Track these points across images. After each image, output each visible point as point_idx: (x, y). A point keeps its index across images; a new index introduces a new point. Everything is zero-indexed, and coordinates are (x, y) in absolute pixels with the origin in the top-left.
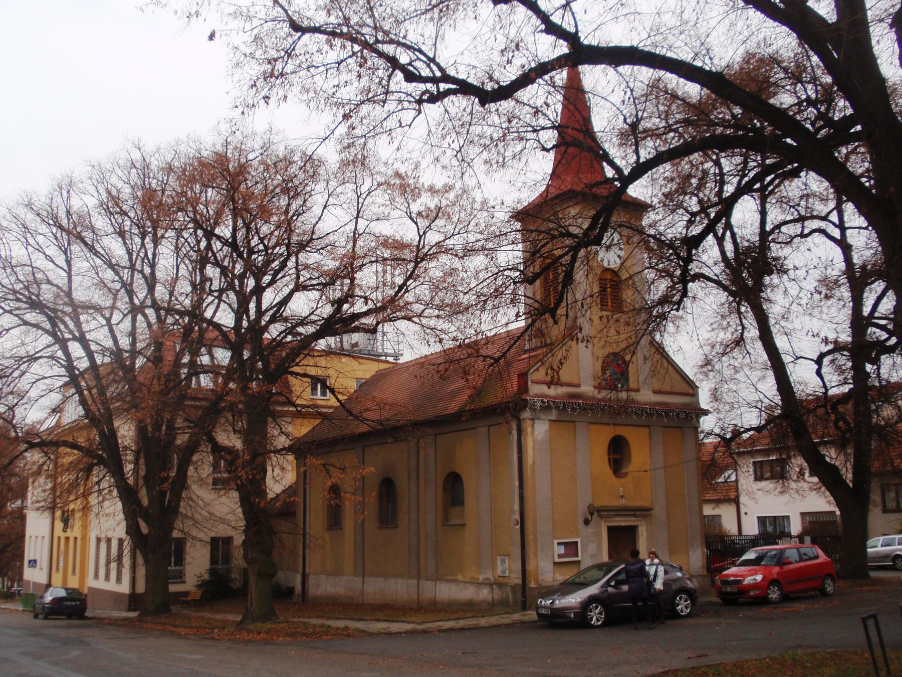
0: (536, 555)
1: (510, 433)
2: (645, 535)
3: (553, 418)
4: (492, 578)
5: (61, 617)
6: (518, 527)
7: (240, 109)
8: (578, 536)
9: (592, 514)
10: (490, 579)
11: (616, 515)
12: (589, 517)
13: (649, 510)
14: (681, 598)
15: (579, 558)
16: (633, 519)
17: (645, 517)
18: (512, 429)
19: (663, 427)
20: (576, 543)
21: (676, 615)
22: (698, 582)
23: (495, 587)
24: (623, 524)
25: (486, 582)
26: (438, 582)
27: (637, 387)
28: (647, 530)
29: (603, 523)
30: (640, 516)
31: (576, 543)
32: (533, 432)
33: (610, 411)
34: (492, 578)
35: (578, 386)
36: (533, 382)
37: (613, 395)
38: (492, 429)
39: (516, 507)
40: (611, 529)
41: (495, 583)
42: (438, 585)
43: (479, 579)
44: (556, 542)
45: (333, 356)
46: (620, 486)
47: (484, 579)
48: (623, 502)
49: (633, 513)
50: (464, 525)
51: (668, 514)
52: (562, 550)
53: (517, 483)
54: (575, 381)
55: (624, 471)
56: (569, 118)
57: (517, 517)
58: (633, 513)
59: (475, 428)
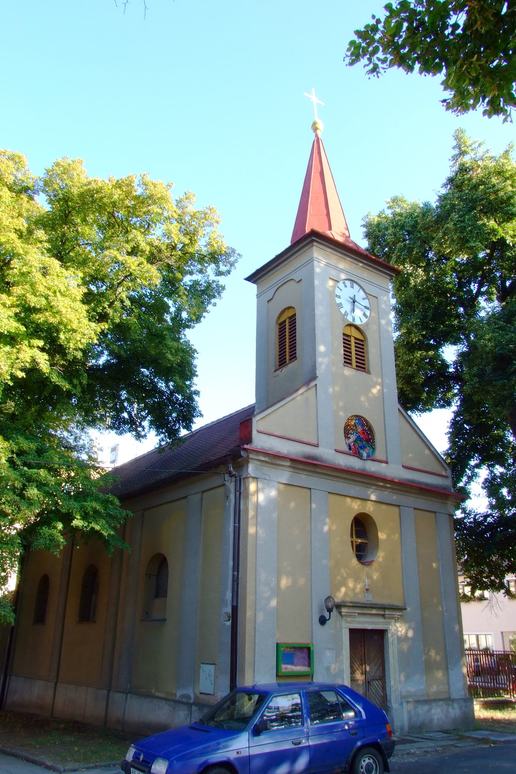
1: (227, 497)
4: (192, 695)
6: (229, 623)
9: (330, 610)
10: (188, 697)
12: (327, 615)
16: (381, 620)
18: (230, 492)
19: (414, 509)
22: (460, 709)
23: (194, 708)
24: (369, 627)
25: (184, 700)
26: (129, 695)
33: (409, 363)
34: (192, 695)
35: (317, 446)
36: (259, 432)
38: (204, 494)
39: (229, 595)
40: (352, 631)
41: (194, 704)
42: (129, 699)
43: (175, 695)
47: (183, 696)
49: (381, 612)
50: (166, 620)
53: (231, 563)
55: (368, 559)
57: (229, 610)
58: (381, 612)
59: (186, 497)
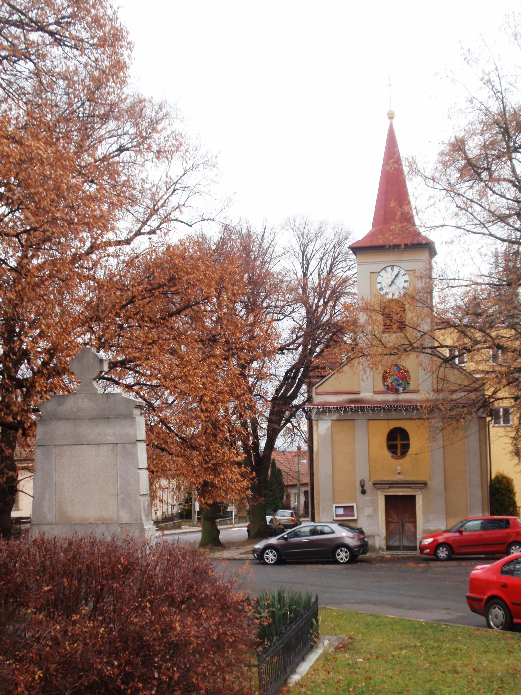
0: (319, 515)
2: (421, 502)
3: (335, 418)
5: (227, 526)
7: (461, 129)
8: (355, 501)
11: (389, 487)
13: (425, 484)
14: (346, 552)
15: (355, 518)
17: (421, 489)
20: (353, 507)
21: (336, 562)
24: (400, 494)
27: (417, 389)
28: (423, 499)
29: (379, 493)
30: (415, 488)
31: (353, 507)
32: (317, 429)
36: (317, 394)
37: (391, 397)
44: (334, 505)
45: (64, 421)
46: (399, 465)
48: (400, 478)
51: (445, 487)
52: (341, 511)
54: (356, 389)
56: (123, 288)
